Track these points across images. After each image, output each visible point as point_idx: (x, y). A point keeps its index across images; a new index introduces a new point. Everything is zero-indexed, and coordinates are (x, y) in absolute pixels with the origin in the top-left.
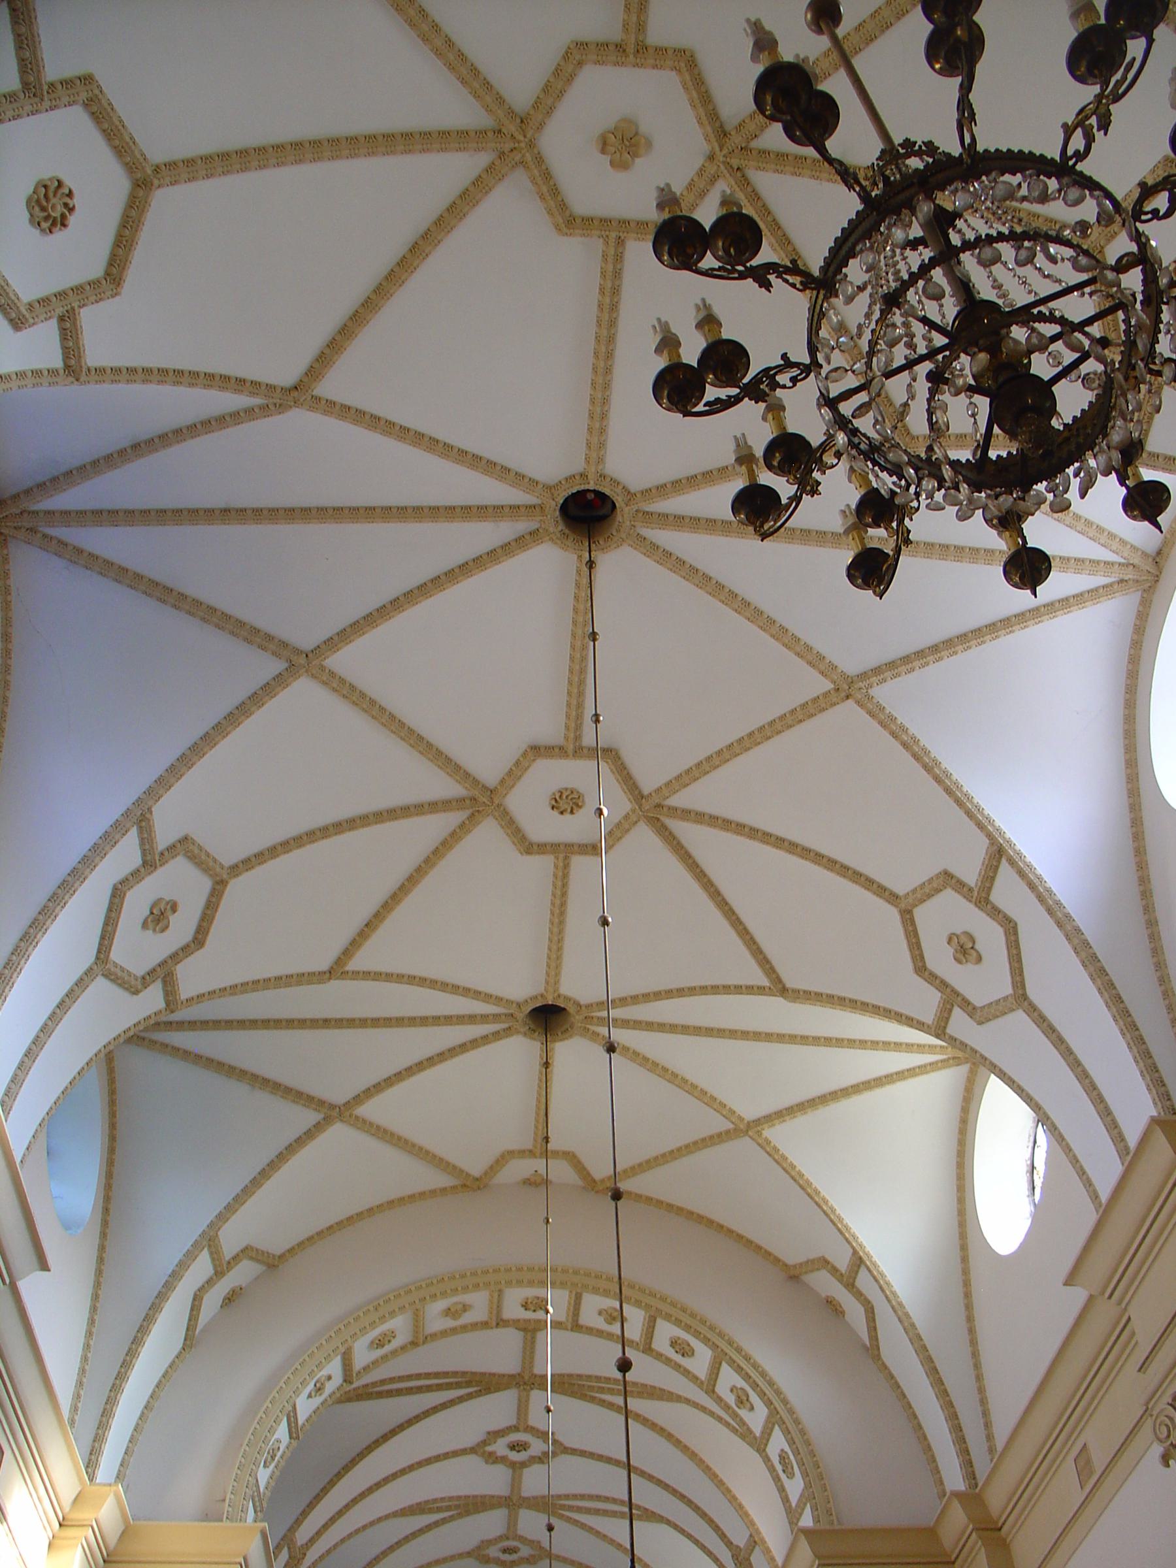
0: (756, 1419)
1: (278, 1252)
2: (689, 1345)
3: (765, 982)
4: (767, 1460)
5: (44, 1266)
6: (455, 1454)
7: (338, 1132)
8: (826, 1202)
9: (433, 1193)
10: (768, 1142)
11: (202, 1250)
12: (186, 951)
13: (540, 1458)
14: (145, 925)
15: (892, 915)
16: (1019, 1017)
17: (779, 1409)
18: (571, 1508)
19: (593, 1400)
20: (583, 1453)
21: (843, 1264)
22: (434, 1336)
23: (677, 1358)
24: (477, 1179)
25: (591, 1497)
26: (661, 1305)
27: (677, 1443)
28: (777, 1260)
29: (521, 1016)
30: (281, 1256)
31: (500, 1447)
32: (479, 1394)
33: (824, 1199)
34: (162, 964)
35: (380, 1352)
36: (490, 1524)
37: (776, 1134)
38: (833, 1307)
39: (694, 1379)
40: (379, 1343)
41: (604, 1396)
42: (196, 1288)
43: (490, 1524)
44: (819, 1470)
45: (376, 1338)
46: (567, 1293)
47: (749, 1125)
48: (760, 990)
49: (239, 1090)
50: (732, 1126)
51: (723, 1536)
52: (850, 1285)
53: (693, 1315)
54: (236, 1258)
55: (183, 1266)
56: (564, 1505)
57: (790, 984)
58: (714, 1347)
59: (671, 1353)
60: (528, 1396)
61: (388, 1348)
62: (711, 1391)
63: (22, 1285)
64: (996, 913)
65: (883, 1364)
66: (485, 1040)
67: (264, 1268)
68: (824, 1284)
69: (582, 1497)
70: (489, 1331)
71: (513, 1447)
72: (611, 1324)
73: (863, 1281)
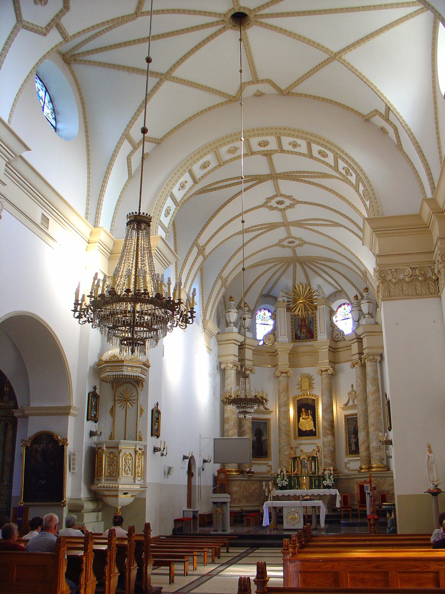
0: (353, 179)
1: (160, 137)
2: (325, 153)
5: (28, 149)
6: (256, 208)
7: (167, 85)
8: (372, 84)
9: (218, 105)
10: (345, 61)
11: (124, 140)
13: (290, 206)
17: (359, 174)
18: (308, 224)
19: (302, 181)
20: (305, 203)
21: (383, 111)
22: (227, 162)
23: (322, 158)
24: (235, 97)
25: (313, 219)
27: (337, 194)
28: (360, 114)
29: (227, 20)
30: (161, 139)
31: (273, 203)
32: (257, 183)
33: (371, 83)
34: (53, 20)
36: (280, 233)
37: (348, 57)
38: (383, 130)
40: (204, 166)
41: (306, 179)
42: (127, 155)
43: (280, 233)
44: (375, 196)
45: (202, 165)
47: (336, 54)
49: (124, 74)
50: (329, 56)
52: (387, 119)
53: (324, 140)
55: (118, 148)
56: (305, 223)
59: (319, 157)
60: (277, 182)
62: (337, 170)
65: (404, 152)
66: (216, 34)
67: (156, 144)
68: (378, 121)
69: (310, 220)
70: (249, 157)
71: (278, 203)
72: (295, 148)
73: (392, 117)
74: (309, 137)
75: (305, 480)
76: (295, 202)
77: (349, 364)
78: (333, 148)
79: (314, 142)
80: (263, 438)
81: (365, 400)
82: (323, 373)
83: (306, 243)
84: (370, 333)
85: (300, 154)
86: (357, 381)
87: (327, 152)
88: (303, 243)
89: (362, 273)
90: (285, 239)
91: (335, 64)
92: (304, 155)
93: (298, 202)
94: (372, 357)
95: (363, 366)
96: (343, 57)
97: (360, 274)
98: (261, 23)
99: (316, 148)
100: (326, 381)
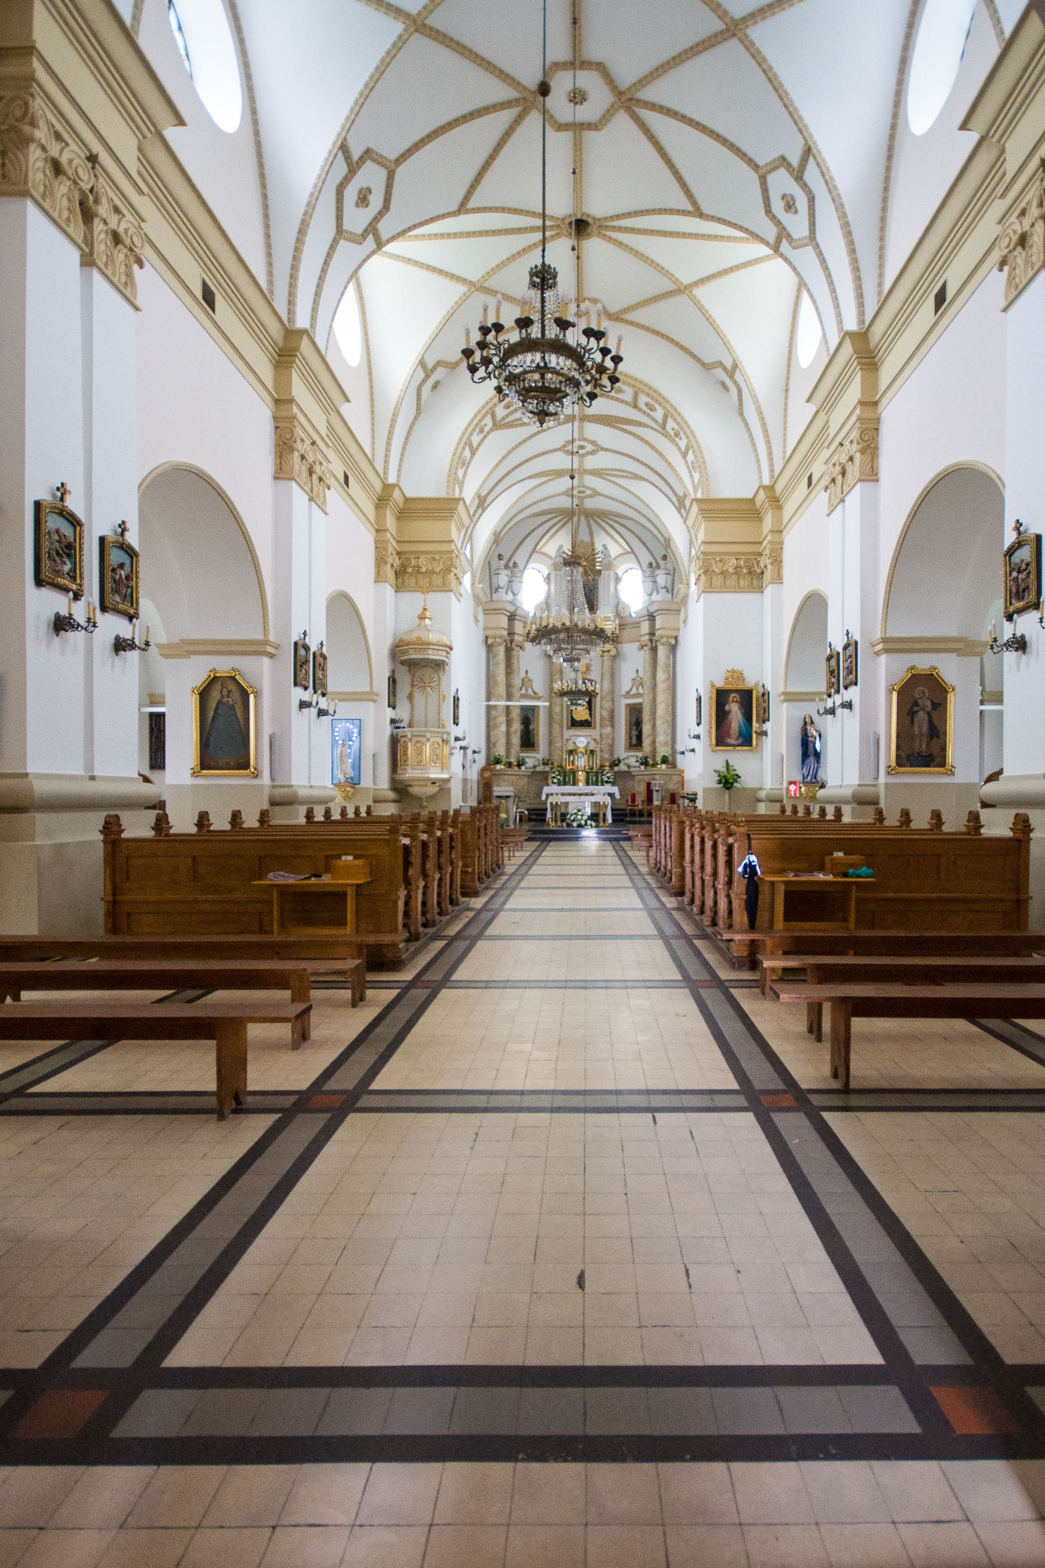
3: (690, 208)
4: (686, 462)
5: (348, 401)
12: (381, 214)
14: (357, 205)
15: (753, 177)
16: (810, 250)
18: (608, 475)
23: (648, 411)
26: (641, 387)
34: (370, 225)
35: (508, 411)
37: (699, 292)
39: (656, 422)
46: (749, 32)
47: (686, 288)
48: (688, 213)
51: (673, 491)
54: (434, 368)
57: (705, 211)
58: (664, 408)
59: (645, 409)
61: (511, 409)
63: (341, 410)
64: (805, 187)
73: (738, 376)
74: (638, 385)
75: (581, 776)
76: (598, 448)
77: (637, 644)
78: (665, 404)
79: (643, 392)
80: (531, 727)
81: (654, 687)
82: (606, 654)
83: (599, 494)
84: (666, 611)
85: (622, 401)
86: (645, 667)
87: (657, 406)
88: (596, 493)
89: (665, 539)
90: (586, 497)
91: (681, 300)
92: (627, 403)
93: (603, 449)
94: (665, 640)
95: (654, 650)
96: (694, 292)
97: (662, 540)
98: (605, 235)
99: (643, 400)
100: (607, 663)
